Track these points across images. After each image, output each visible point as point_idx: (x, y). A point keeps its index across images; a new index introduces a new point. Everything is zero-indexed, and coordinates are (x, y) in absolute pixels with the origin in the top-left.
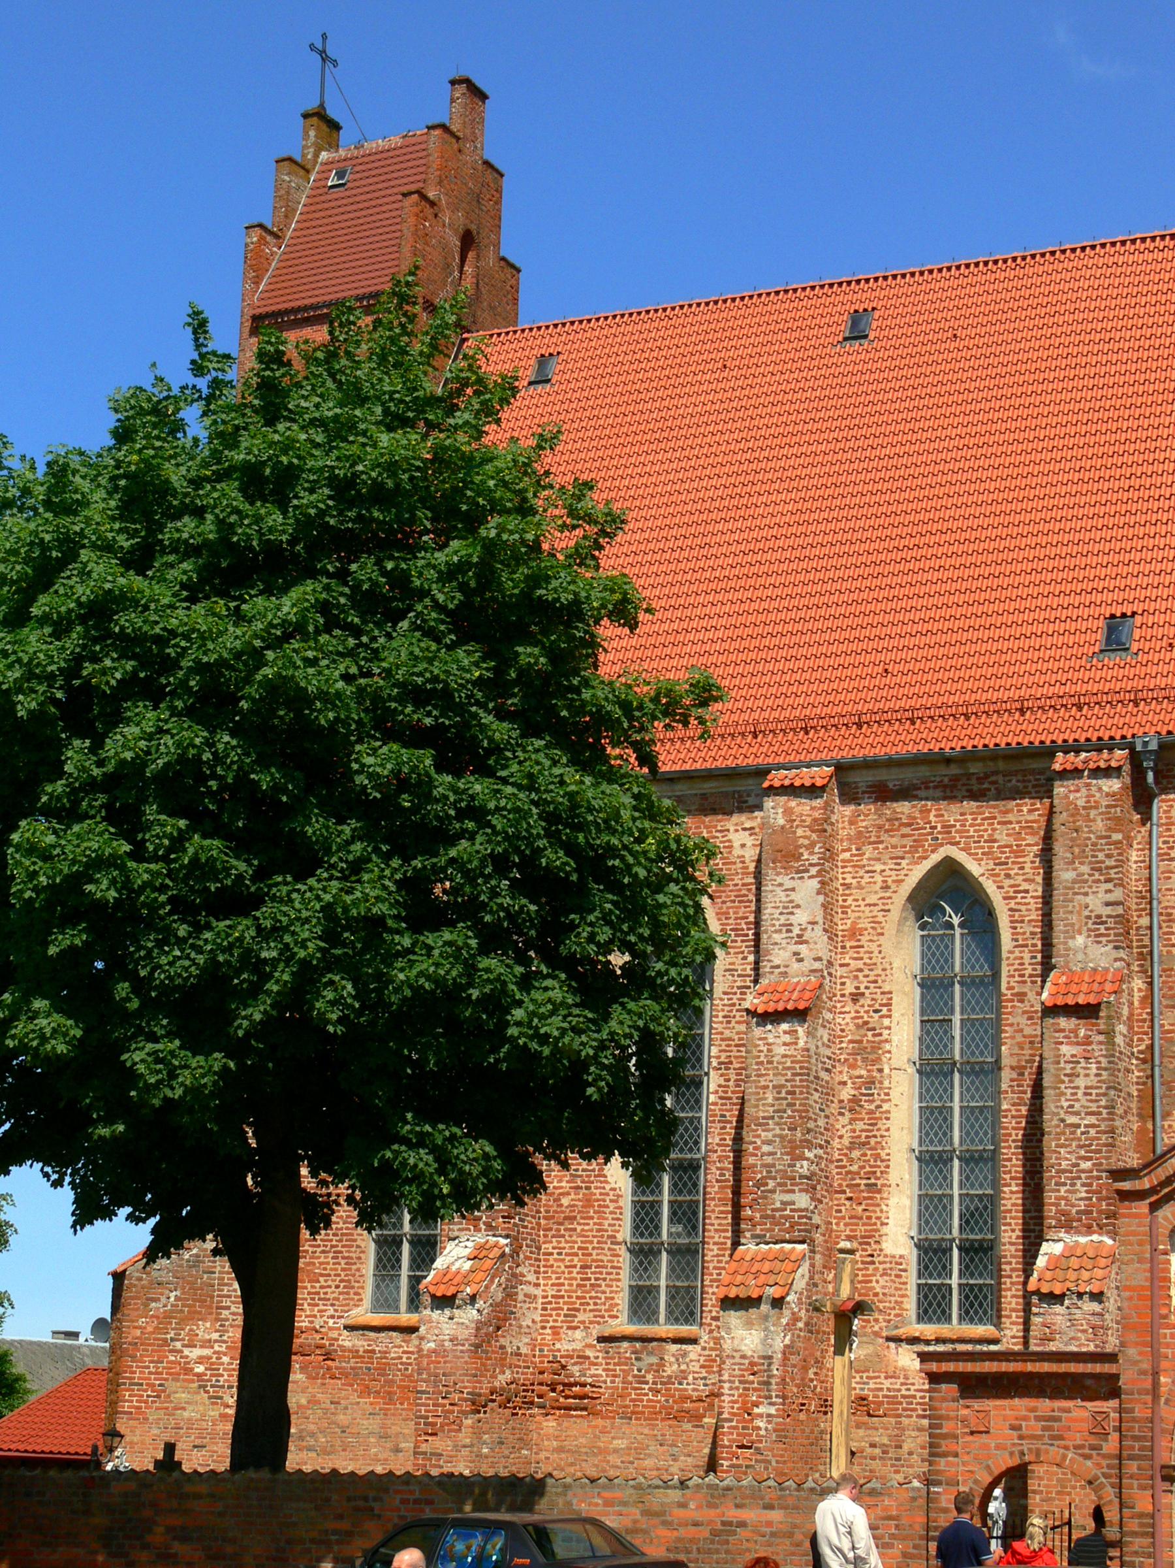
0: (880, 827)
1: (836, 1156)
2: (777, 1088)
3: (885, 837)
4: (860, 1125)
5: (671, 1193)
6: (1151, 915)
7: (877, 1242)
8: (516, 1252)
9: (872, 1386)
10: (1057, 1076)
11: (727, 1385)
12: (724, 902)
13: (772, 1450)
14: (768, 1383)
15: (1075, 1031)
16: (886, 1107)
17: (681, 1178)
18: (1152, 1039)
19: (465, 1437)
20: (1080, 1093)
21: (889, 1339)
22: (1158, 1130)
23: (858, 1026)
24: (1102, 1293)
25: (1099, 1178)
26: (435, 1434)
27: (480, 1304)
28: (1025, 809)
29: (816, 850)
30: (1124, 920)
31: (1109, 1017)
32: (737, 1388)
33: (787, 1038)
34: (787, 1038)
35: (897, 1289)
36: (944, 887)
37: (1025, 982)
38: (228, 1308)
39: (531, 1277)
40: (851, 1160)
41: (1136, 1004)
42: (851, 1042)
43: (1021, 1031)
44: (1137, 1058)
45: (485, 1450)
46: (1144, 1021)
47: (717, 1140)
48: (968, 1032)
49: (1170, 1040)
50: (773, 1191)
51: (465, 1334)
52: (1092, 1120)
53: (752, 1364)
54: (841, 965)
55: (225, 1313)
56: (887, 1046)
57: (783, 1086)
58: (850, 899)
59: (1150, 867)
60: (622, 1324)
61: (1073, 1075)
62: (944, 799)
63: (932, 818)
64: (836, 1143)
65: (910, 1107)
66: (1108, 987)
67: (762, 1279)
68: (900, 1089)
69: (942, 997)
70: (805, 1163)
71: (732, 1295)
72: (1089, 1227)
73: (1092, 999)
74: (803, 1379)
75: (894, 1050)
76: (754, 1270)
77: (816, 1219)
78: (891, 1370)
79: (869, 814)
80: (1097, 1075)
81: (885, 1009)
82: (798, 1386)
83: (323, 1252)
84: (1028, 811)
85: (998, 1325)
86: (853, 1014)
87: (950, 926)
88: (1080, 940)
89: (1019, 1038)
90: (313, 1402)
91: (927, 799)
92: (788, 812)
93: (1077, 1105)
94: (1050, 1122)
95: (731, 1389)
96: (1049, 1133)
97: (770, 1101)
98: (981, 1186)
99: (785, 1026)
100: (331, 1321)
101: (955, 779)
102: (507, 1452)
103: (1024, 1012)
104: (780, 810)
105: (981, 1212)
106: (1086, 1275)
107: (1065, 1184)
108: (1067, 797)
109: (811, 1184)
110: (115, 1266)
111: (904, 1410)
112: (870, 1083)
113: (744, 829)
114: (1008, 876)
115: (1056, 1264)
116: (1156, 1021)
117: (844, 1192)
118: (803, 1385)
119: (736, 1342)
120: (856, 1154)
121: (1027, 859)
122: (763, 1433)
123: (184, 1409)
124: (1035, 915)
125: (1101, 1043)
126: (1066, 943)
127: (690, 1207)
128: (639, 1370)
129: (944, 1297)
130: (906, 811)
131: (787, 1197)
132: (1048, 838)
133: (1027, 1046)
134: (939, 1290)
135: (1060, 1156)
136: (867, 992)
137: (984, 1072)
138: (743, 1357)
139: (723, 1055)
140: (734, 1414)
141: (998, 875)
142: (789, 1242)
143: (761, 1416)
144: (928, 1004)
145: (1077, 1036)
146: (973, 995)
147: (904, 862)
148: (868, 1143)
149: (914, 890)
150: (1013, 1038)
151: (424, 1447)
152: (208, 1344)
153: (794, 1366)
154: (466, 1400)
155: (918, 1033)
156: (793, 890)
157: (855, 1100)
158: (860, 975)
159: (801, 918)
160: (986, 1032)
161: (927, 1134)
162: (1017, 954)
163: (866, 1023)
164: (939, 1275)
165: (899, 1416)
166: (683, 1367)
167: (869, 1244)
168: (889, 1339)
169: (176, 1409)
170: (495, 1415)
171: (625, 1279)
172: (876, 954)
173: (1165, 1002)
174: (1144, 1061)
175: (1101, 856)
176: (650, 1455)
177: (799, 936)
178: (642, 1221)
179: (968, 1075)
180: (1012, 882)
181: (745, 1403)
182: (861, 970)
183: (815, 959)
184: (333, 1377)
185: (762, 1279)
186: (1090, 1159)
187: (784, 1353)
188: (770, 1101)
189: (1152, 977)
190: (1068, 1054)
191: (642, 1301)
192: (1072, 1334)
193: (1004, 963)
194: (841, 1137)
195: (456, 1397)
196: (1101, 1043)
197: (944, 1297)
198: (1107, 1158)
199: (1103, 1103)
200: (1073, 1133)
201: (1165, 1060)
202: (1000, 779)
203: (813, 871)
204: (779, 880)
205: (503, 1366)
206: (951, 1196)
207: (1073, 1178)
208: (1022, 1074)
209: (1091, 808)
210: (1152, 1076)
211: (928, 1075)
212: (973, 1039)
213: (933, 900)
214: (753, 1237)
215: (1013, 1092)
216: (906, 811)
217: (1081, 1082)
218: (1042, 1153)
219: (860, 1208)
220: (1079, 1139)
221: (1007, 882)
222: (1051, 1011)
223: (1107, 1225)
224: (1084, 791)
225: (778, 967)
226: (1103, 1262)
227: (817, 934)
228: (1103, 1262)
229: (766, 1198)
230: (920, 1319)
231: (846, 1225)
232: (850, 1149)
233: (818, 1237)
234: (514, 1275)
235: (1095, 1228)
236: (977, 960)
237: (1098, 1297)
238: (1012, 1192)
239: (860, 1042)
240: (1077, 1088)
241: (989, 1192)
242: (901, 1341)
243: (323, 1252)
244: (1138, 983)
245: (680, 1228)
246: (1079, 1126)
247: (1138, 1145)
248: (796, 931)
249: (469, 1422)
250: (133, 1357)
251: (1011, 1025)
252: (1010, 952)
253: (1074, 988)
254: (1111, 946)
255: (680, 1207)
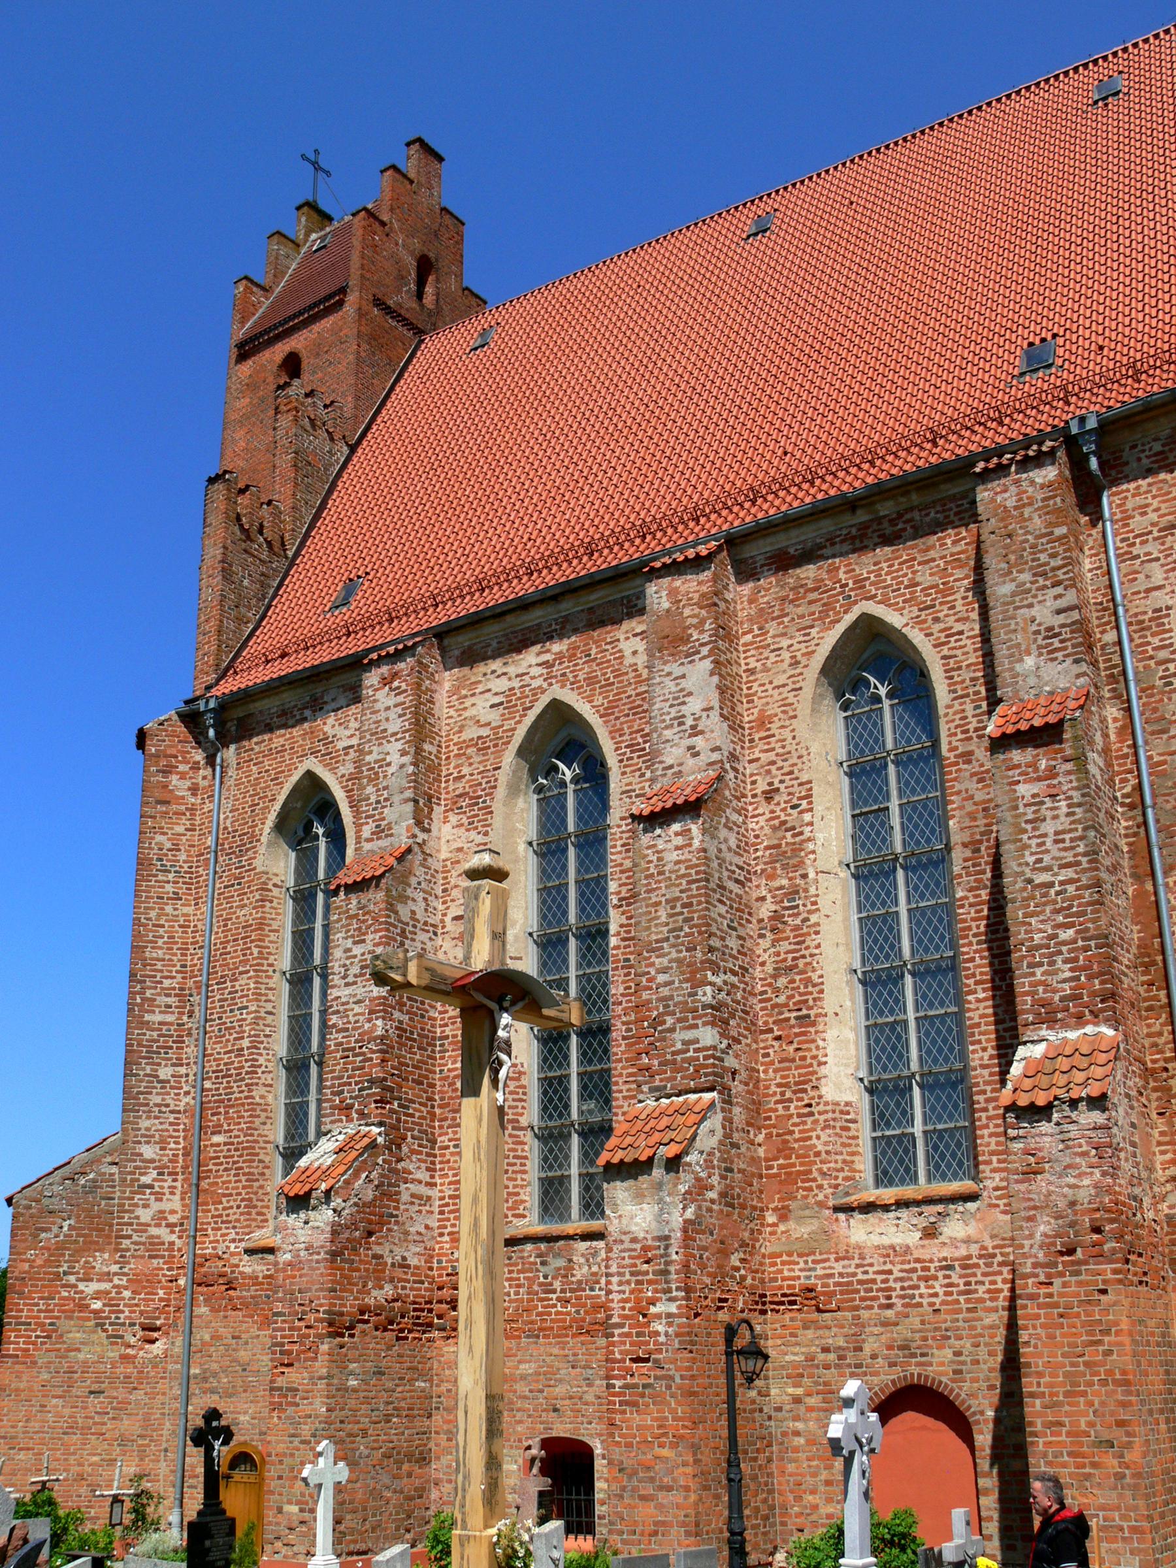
0: (783, 599)
1: (759, 988)
2: (672, 902)
3: (789, 608)
4: (785, 946)
5: (580, 1063)
6: (1118, 628)
7: (815, 1088)
8: (395, 1142)
9: (820, 1272)
10: (1016, 825)
11: (615, 1280)
12: (617, 718)
13: (674, 1361)
14: (665, 1272)
15: (1034, 765)
16: (814, 919)
17: (590, 1045)
18: (1139, 776)
19: (321, 1367)
20: (1049, 842)
21: (837, 1209)
22: (1161, 890)
23: (774, 829)
24: (1104, 1096)
25: (1086, 949)
26: (290, 1365)
27: (337, 1202)
28: (949, 541)
29: (707, 627)
30: (1082, 627)
31: (1076, 738)
32: (628, 1282)
33: (679, 841)
34: (679, 841)
35: (844, 1145)
36: (865, 656)
37: (970, 738)
38: (130, 1237)
39: (423, 1175)
40: (777, 991)
41: (1113, 737)
42: (767, 848)
43: (972, 797)
44: (1123, 805)
45: (353, 1383)
46: (1126, 756)
47: (621, 990)
48: (910, 819)
49: (1163, 774)
50: (672, 1030)
51: (322, 1239)
52: (1070, 873)
53: (645, 1249)
54: (750, 762)
55: (126, 1243)
56: (811, 846)
57: (678, 899)
58: (755, 685)
59: (1109, 573)
60: (531, 1223)
61: (1037, 820)
62: (854, 551)
63: (842, 576)
64: (758, 972)
65: (846, 919)
66: (1072, 704)
67: (657, 1137)
68: (831, 897)
69: (874, 783)
70: (708, 989)
71: (615, 1160)
72: (1080, 1016)
73: (1052, 719)
74: (720, 1267)
75: (819, 850)
76: (647, 1129)
77: (730, 1062)
78: (842, 1248)
79: (770, 587)
80: (1068, 815)
81: (804, 802)
82: (712, 1275)
83: (226, 1170)
84: (952, 544)
85: (976, 1178)
86: (768, 816)
87: (877, 699)
88: (1030, 662)
89: (970, 807)
90: (216, 1337)
91: (834, 556)
92: (673, 592)
93: (1047, 858)
94: (1013, 886)
95: (620, 1284)
96: (1014, 901)
97: (663, 919)
98: (942, 1004)
99: (676, 827)
100: (233, 1246)
101: (863, 527)
102: (390, 1384)
103: (973, 775)
104: (664, 593)
105: (946, 1034)
106: (1079, 1077)
107: (1041, 964)
108: (993, 500)
109: (719, 1016)
110: (8, 1194)
111: (862, 1299)
112: (793, 893)
113: (635, 635)
114: (936, 620)
115: (1035, 1070)
116: (1141, 752)
117: (771, 1031)
118: (722, 1274)
119: (624, 1221)
120: (782, 982)
121: (958, 596)
122: (662, 1339)
123: (78, 1350)
124: (974, 658)
125: (1069, 773)
126: (1012, 669)
127: (601, 1078)
128: (546, 1277)
129: (906, 1151)
130: (812, 575)
131: (689, 1035)
132: (979, 568)
133: (980, 815)
134: (900, 1142)
135: (1031, 928)
136: (782, 787)
137: (930, 864)
138: (634, 1240)
139: (624, 889)
140: (626, 1317)
141: (925, 621)
142: (695, 1091)
143: (658, 1316)
144: (860, 795)
145: (1036, 770)
146: (912, 774)
147: (814, 631)
148: (796, 967)
149: (828, 658)
150: (961, 808)
151: (280, 1382)
152: (107, 1277)
153: (705, 1249)
154: (321, 1320)
155: (850, 831)
156: (683, 676)
157: (776, 917)
158: (773, 768)
159: (694, 705)
160: (931, 814)
161: (871, 950)
162: (957, 707)
163: (784, 823)
164: (899, 1124)
165: (857, 1308)
166: (595, 1269)
167: (805, 1091)
168: (837, 1209)
169: (69, 1350)
170: (370, 1343)
171: (533, 1171)
172: (790, 740)
173: (1149, 729)
174: (1132, 807)
175: (1043, 557)
176: (560, 1381)
177: (693, 727)
178: (551, 1100)
179: (914, 869)
180: (942, 626)
181: (638, 1301)
182: (773, 763)
183: (713, 750)
184: (235, 1309)
185: (657, 1137)
186: (1072, 925)
187: (685, 1231)
188: (663, 919)
189: (1129, 701)
190: (1028, 795)
191: (552, 1193)
192: (1068, 1160)
193: (942, 722)
194: (763, 964)
195: (311, 1317)
196: (1069, 773)
197: (906, 1151)
198: (1094, 921)
199: (1081, 850)
200: (1045, 895)
201: (1160, 800)
202: (916, 515)
203: (705, 651)
204: (667, 669)
205: (379, 1279)
206: (906, 1022)
207: (1052, 955)
208: (978, 850)
209: (1024, 506)
210: (1145, 823)
211: (865, 878)
212: (916, 826)
213: (854, 673)
214: (651, 1090)
215: (968, 874)
216: (812, 575)
217: (1049, 827)
218: (1007, 930)
219: (791, 1048)
220: (1055, 902)
221: (937, 627)
222: (1000, 744)
223: (1103, 1010)
224: (1013, 489)
225: (671, 767)
226: (1102, 1058)
227: (714, 725)
228: (1102, 1058)
229: (664, 1039)
230: (878, 1183)
231: (775, 1071)
232: (775, 977)
233: (737, 1087)
234: (396, 1171)
235: (1088, 1017)
236: (913, 732)
237: (1099, 1102)
238: (978, 1001)
239: (779, 846)
240: (1045, 835)
241: (954, 1009)
242: (853, 1209)
243: (226, 1170)
244: (1112, 712)
245: (592, 1105)
246: (1052, 885)
247: (1137, 914)
248: (689, 722)
249: (324, 1348)
250: (21, 1293)
251: (958, 793)
252: (948, 707)
253: (1028, 715)
254: (1069, 660)
255: (591, 1079)
